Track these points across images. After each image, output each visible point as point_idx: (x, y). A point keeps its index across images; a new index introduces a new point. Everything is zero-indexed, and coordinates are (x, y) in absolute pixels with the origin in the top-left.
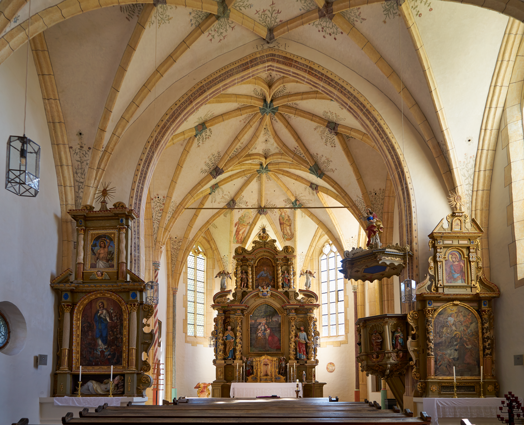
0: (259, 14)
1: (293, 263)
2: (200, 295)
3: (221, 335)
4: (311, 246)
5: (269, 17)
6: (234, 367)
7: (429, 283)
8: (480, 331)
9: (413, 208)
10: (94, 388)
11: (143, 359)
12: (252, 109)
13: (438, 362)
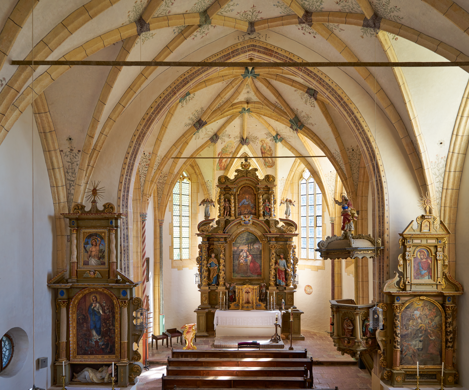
1: (273, 193)
2: (185, 218)
3: (205, 262)
4: (291, 171)
7: (398, 279)
8: (444, 324)
9: (385, 201)
10: (91, 377)
11: (135, 349)
13: (403, 353)
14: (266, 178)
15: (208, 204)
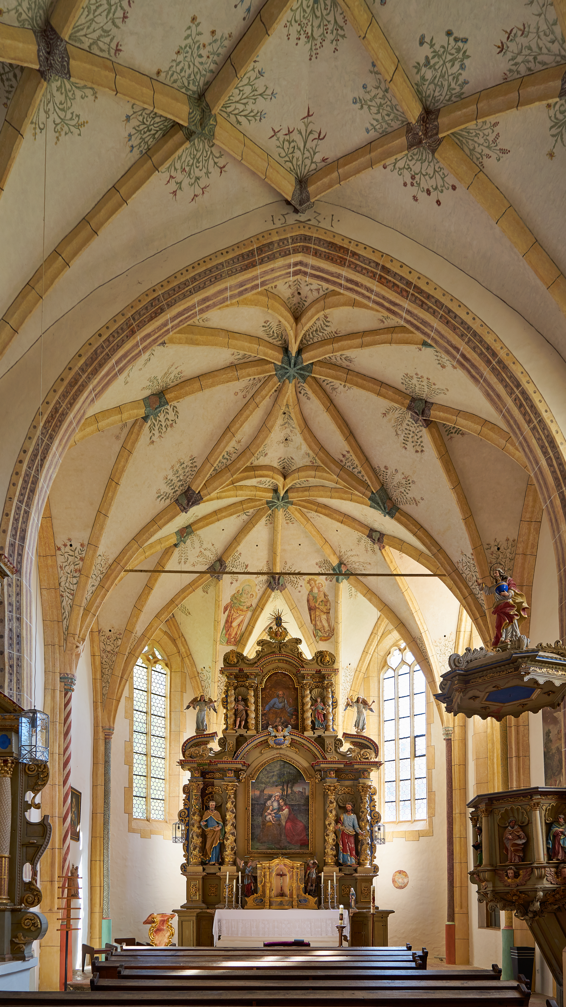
0: (278, 139)
1: (332, 684)
3: (196, 818)
4: (365, 652)
5: (299, 149)
6: (221, 879)
11: (27, 878)
12: (259, 368)
14: (317, 658)
15: (204, 705)
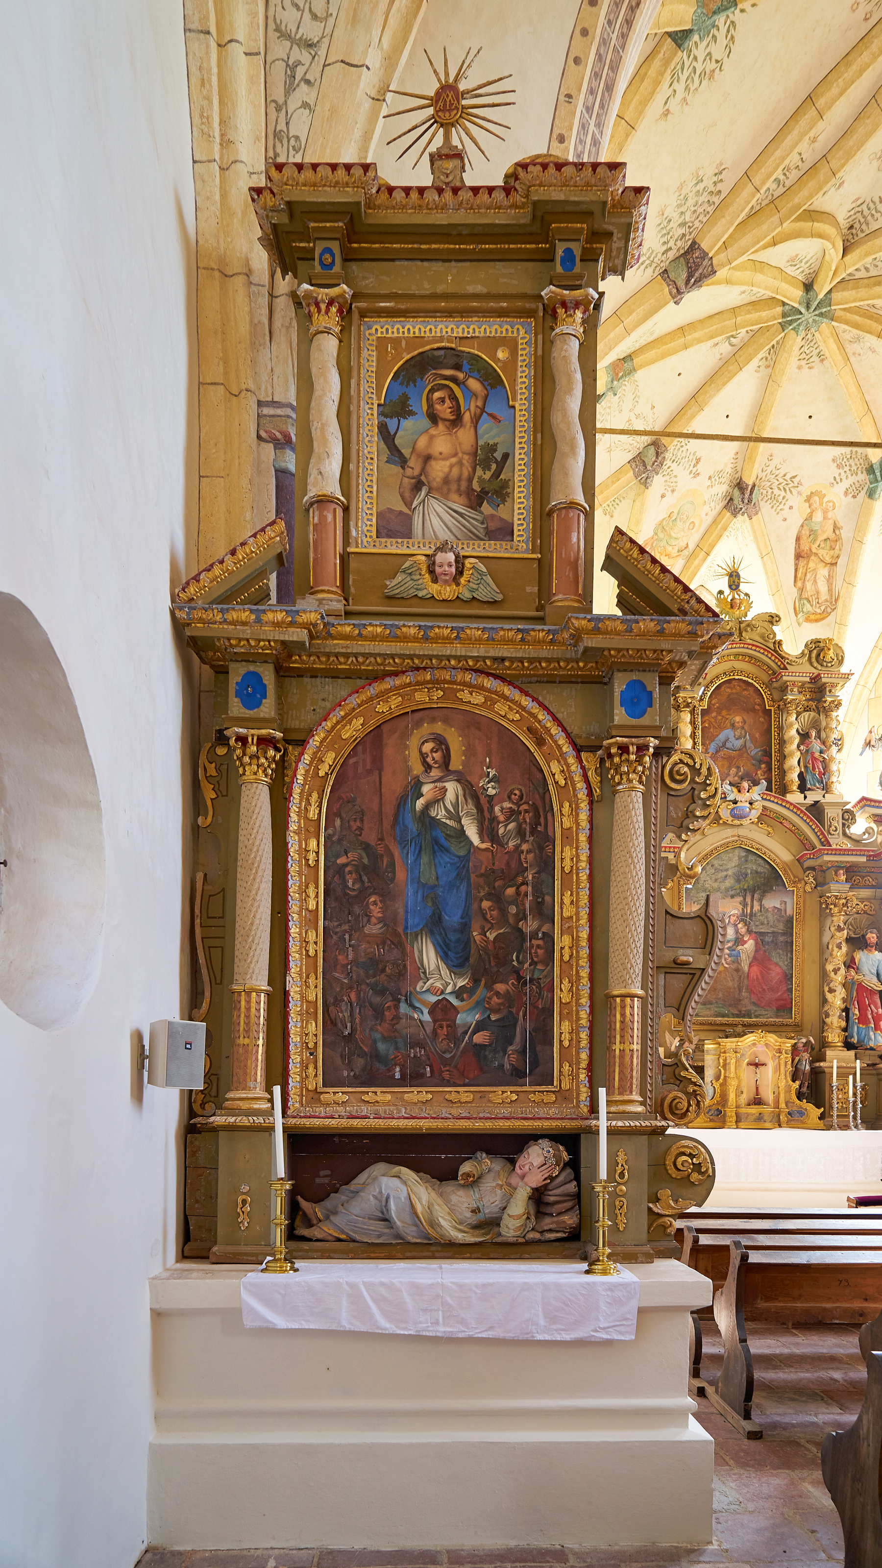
10: (419, 1209)
14: (811, 652)
